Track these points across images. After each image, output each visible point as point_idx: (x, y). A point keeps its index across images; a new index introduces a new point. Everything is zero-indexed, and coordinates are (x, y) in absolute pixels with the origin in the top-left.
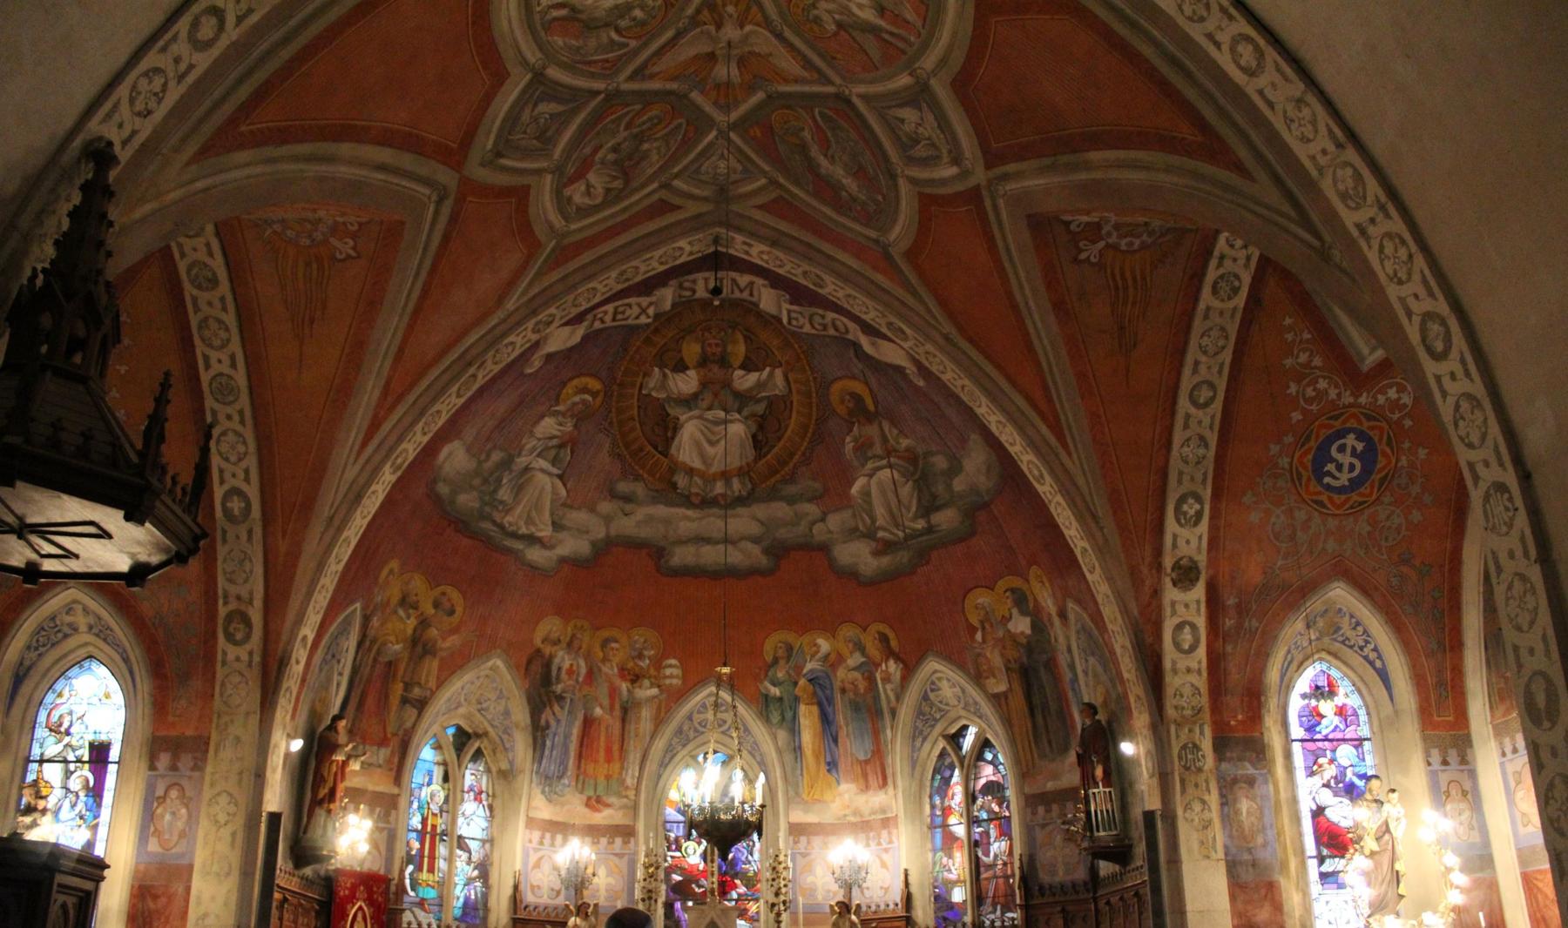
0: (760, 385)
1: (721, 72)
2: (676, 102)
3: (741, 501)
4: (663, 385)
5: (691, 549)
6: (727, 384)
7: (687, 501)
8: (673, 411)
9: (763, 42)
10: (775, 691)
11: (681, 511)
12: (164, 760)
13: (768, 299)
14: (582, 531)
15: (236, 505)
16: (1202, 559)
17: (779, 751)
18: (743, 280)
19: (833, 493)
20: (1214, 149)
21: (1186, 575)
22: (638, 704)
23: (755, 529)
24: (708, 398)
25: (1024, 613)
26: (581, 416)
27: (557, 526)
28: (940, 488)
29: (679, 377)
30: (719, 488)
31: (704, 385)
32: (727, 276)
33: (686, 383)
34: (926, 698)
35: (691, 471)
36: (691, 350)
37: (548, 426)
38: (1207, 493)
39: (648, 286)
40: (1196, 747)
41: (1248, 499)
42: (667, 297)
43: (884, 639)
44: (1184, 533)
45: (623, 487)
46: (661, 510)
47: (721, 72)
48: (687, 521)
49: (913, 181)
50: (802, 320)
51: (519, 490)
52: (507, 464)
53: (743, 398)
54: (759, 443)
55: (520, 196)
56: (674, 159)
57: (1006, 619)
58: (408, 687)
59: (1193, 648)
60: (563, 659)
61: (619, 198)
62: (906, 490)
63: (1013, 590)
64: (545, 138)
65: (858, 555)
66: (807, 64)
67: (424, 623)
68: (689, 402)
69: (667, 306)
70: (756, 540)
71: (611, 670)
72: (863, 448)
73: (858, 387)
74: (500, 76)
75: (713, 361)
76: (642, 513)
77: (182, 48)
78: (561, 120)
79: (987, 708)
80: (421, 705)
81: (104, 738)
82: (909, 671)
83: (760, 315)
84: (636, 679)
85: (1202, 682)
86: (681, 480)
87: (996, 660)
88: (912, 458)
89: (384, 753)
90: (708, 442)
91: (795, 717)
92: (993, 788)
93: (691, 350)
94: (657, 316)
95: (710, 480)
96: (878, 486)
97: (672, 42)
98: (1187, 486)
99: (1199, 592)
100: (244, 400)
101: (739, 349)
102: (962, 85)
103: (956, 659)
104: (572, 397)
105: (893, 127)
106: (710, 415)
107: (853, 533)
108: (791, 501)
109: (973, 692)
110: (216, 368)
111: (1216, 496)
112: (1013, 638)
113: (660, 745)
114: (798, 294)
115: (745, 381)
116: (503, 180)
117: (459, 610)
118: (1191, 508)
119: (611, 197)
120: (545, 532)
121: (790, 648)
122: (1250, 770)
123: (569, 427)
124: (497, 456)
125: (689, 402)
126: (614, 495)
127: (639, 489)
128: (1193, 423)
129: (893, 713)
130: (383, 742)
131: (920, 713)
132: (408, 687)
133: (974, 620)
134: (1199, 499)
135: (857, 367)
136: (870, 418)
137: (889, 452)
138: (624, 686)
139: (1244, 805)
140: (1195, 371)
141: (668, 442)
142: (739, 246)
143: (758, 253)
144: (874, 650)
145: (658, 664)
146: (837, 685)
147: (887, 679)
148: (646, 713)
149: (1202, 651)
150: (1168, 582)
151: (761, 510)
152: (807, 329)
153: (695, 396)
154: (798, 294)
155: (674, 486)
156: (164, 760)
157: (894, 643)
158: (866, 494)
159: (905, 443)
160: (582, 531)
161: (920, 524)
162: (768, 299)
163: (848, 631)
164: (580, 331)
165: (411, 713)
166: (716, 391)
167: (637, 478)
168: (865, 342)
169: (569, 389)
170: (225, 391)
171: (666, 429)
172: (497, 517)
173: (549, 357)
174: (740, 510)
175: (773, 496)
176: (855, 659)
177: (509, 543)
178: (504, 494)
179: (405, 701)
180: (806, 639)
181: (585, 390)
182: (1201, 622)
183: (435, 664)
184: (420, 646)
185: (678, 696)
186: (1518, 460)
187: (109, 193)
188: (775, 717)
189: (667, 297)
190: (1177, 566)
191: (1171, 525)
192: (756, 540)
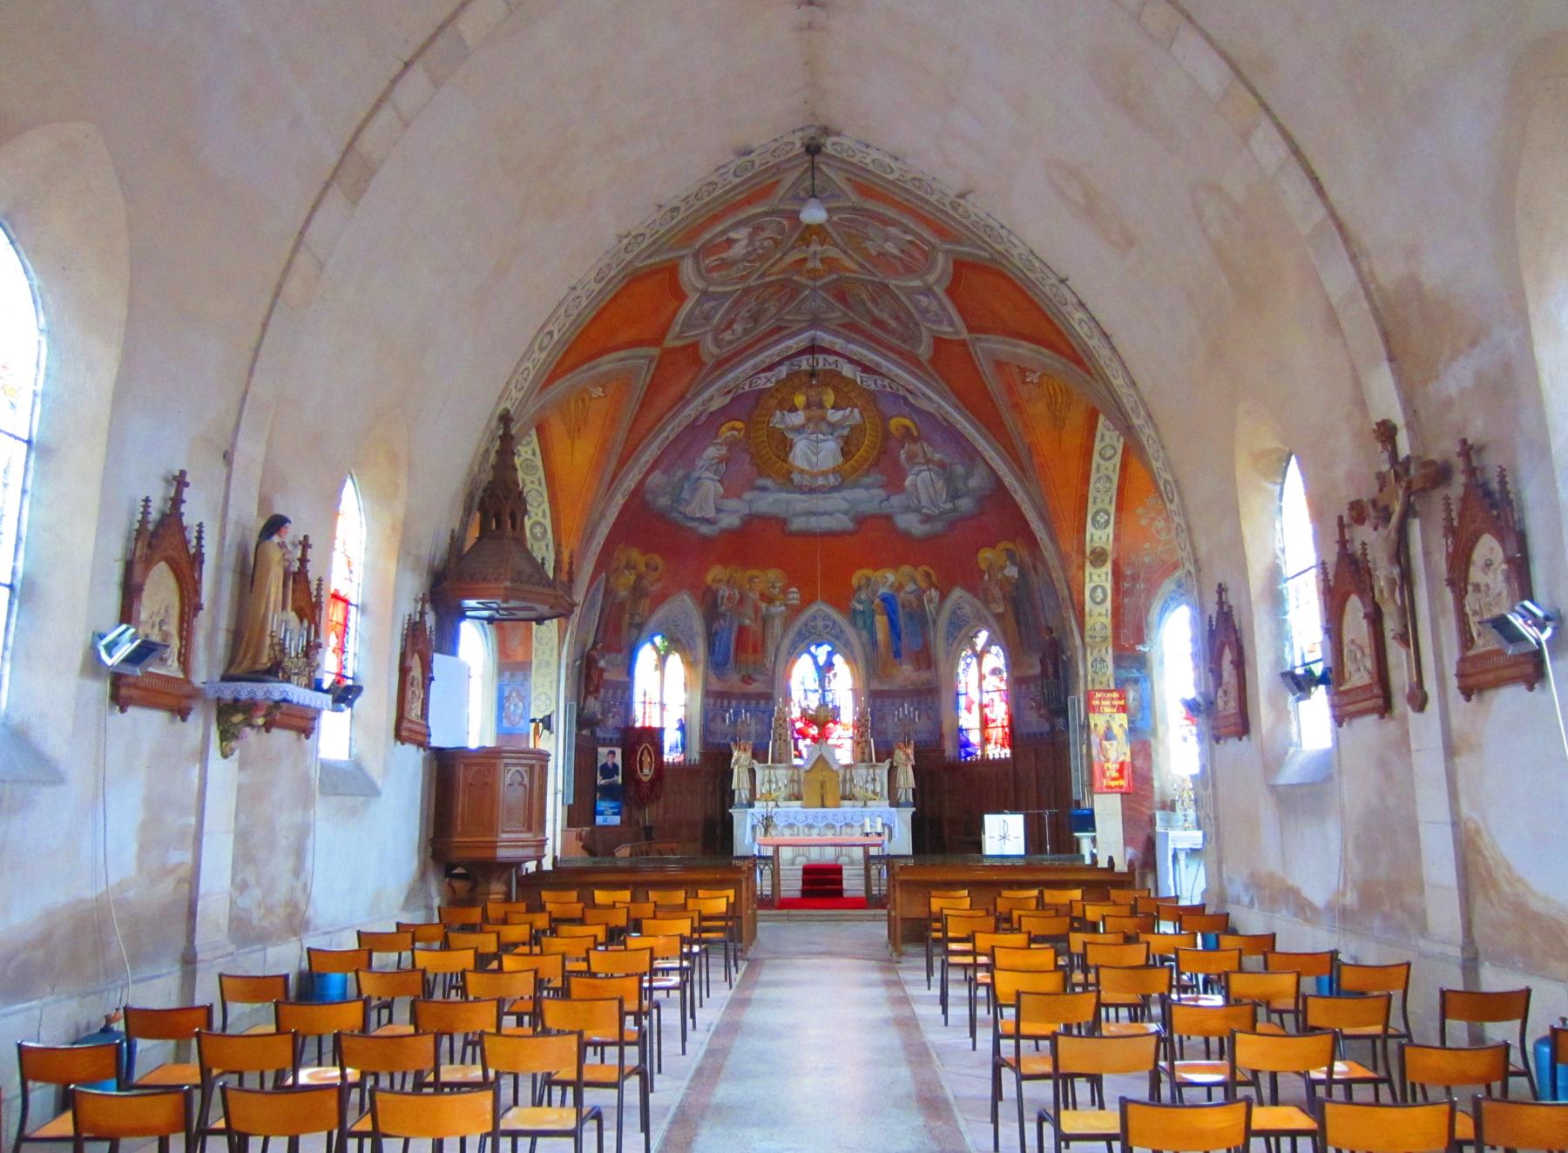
0: (845, 418)
1: (810, 265)
2: (783, 284)
3: (834, 489)
4: (783, 420)
5: (803, 519)
6: (824, 419)
7: (801, 490)
8: (789, 435)
9: (833, 252)
10: (860, 607)
11: (797, 496)
12: (507, 674)
13: (847, 370)
14: (733, 512)
15: (538, 530)
16: (1109, 547)
17: (863, 646)
18: (832, 359)
19: (895, 483)
20: (1079, 362)
21: (1099, 557)
22: (773, 617)
23: (844, 506)
24: (811, 426)
25: (1014, 563)
26: (732, 444)
27: (719, 510)
28: (960, 485)
29: (793, 415)
30: (821, 481)
31: (809, 420)
32: (821, 357)
33: (798, 418)
34: (954, 613)
35: (802, 471)
36: (800, 400)
37: (712, 452)
38: (1112, 510)
39: (770, 368)
40: (1103, 660)
41: (1140, 511)
42: (783, 371)
43: (928, 575)
44: (1097, 533)
45: (760, 482)
46: (784, 496)
47: (810, 265)
48: (800, 502)
49: (947, 252)
50: (870, 383)
51: (695, 490)
52: (686, 477)
53: (833, 426)
54: (846, 453)
55: (694, 347)
56: (781, 309)
57: (1002, 568)
58: (632, 617)
59: (1103, 601)
60: (724, 591)
61: (751, 330)
62: (940, 484)
63: (1007, 550)
64: (707, 318)
65: (909, 523)
66: (861, 266)
67: (640, 577)
68: (799, 430)
69: (784, 375)
70: (845, 513)
71: (754, 596)
72: (911, 457)
73: (907, 422)
74: (681, 297)
75: (814, 405)
76: (770, 497)
77: (536, 355)
78: (715, 309)
79: (992, 621)
80: (640, 627)
81: (828, 856)
82: (943, 597)
83: (843, 378)
84: (770, 600)
85: (1108, 621)
86: (796, 478)
87: (997, 592)
88: (942, 465)
89: (620, 657)
90: (814, 453)
91: (873, 623)
92: (995, 672)
93: (800, 400)
94: (778, 382)
95: (814, 476)
96: (921, 481)
97: (781, 259)
98: (1099, 505)
99: (1108, 568)
100: (541, 473)
101: (829, 398)
102: (950, 292)
103: (971, 588)
104: (726, 432)
105: (916, 304)
106: (813, 437)
107: (907, 509)
108: (867, 487)
109: (984, 611)
110: (524, 456)
111: (1119, 509)
112: (1007, 579)
113: (786, 643)
114: (866, 369)
115: (834, 416)
116: (686, 342)
117: (661, 567)
118: (1102, 518)
119: (745, 331)
120: (711, 514)
121: (868, 579)
122: (1135, 674)
123: (724, 451)
124: (680, 473)
125: (799, 430)
126: (753, 488)
127: (769, 483)
128: (1102, 469)
129: (935, 622)
130: (619, 651)
131: (951, 623)
132: (632, 617)
133: (983, 566)
134: (1108, 513)
135: (906, 410)
136: (915, 440)
137: (928, 461)
138: (763, 606)
139: (1131, 695)
140: (1102, 439)
141: (787, 454)
142: (825, 339)
143: (839, 344)
144: (923, 584)
145: (784, 591)
146: (899, 602)
147: (930, 600)
148: (778, 622)
149: (1108, 604)
150: (1088, 564)
151: (849, 494)
152: (873, 387)
153: (803, 426)
154: (866, 369)
155: (791, 481)
156: (507, 674)
157: (934, 579)
158: (915, 485)
159: (937, 456)
160: (733, 512)
161: (949, 506)
162: (847, 370)
163: (906, 569)
164: (728, 399)
165: (635, 632)
166: (817, 421)
167: (768, 476)
168: (911, 399)
169: (724, 429)
170: (530, 467)
171: (786, 446)
172: (681, 508)
173: (711, 414)
174: (835, 495)
175: (856, 485)
176: (911, 587)
177: (690, 524)
178: (686, 495)
179: (631, 625)
180: (880, 573)
181: (733, 429)
182: (1109, 586)
183: (648, 601)
184: (638, 591)
185: (796, 611)
186: (1196, 561)
187: (512, 438)
188: (860, 623)
189: (783, 371)
190: (1093, 552)
191: (1090, 528)
192: (845, 513)
